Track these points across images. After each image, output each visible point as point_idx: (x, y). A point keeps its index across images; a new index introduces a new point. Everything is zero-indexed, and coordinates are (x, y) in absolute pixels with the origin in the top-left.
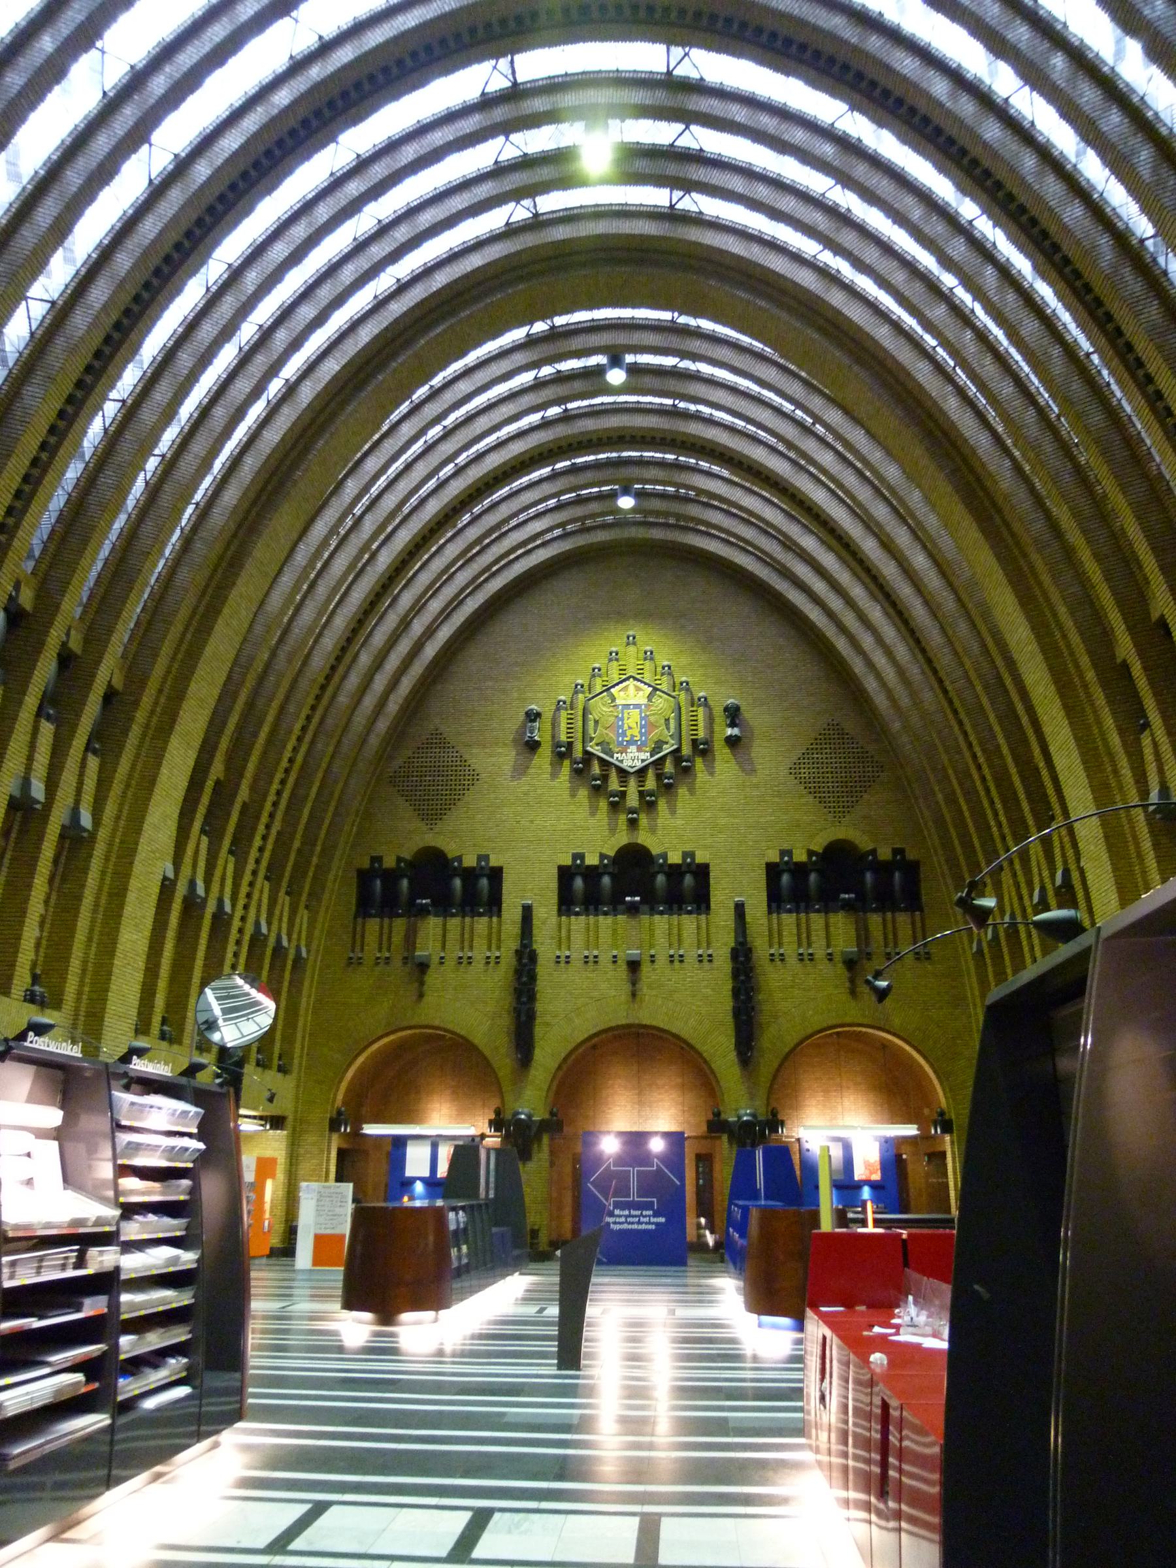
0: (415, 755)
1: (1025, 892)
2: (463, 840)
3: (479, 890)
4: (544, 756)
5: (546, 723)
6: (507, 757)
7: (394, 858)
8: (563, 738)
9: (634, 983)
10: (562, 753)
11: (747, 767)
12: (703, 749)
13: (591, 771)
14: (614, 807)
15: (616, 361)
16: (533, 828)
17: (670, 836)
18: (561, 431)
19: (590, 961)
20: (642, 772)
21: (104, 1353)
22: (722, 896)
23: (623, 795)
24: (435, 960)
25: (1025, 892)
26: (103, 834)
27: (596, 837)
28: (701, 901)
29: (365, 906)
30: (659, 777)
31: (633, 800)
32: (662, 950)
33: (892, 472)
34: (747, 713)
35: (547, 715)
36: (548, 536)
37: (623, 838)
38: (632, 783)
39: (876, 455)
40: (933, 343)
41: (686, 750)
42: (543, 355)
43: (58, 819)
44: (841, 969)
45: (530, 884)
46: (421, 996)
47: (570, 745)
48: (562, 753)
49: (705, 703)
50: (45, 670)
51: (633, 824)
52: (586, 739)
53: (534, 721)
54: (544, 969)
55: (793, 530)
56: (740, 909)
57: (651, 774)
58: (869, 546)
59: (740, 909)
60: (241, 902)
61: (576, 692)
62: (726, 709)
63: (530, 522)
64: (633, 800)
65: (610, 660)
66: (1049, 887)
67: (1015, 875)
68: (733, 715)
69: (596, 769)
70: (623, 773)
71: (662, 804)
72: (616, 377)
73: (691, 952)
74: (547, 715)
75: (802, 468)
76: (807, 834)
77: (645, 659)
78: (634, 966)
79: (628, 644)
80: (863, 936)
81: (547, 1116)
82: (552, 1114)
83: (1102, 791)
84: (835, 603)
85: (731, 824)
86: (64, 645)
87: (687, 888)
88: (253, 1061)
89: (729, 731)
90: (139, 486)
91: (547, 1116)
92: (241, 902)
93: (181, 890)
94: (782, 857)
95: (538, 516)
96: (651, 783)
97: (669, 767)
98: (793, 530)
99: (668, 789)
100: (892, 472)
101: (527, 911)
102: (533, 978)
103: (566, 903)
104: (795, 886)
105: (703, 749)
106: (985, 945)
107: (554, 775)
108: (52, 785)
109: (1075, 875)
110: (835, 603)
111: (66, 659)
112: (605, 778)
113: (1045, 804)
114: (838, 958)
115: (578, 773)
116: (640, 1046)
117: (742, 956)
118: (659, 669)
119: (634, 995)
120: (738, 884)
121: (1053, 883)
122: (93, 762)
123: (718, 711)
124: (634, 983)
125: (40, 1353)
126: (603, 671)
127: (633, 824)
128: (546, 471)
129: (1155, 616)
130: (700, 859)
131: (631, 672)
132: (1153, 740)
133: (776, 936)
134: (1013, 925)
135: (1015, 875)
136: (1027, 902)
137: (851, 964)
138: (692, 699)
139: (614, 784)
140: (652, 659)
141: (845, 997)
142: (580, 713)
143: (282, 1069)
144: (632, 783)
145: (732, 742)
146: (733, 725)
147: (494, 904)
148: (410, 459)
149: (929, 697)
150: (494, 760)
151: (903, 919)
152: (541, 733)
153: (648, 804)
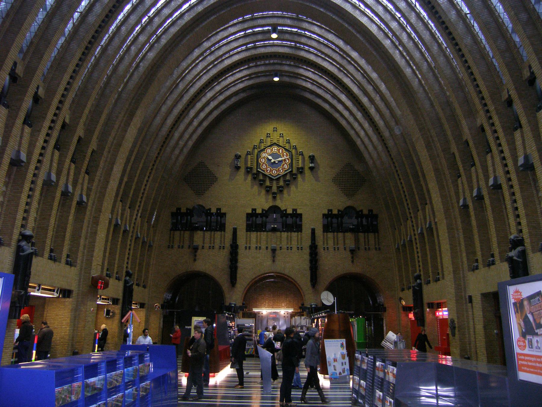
0: (198, 176)
1: (415, 228)
2: (213, 200)
3: (216, 221)
4: (243, 170)
5: (242, 160)
6: (228, 170)
7: (185, 208)
8: (249, 165)
9: (274, 257)
10: (249, 170)
11: (317, 179)
12: (301, 171)
13: (258, 177)
14: (267, 191)
15: (274, 31)
16: (237, 197)
17: (287, 202)
18: (254, 52)
19: (258, 248)
20: (278, 179)
21: (88, 378)
22: (307, 225)
23: (271, 187)
24: (200, 247)
25: (415, 228)
26: (90, 204)
27: (262, 203)
28: (298, 228)
29: (175, 228)
30: (285, 181)
31: (274, 189)
32: (284, 245)
33: (374, 75)
34: (318, 159)
35: (243, 157)
36: (239, 49)
37: (270, 203)
38: (275, 182)
39: (368, 69)
40: (399, 16)
41: (295, 171)
42: (251, 40)
43: (76, 199)
44: (349, 253)
45: (236, 219)
46: (195, 260)
47: (251, 168)
48: (249, 170)
49: (302, 154)
50: (28, 102)
51: (274, 198)
52: (258, 164)
53: (239, 158)
54: (320, 250)
55: (337, 92)
56: (313, 231)
57: (282, 180)
58: (365, 100)
59: (313, 231)
60: (132, 225)
61: (254, 148)
62: (310, 157)
63: (238, 80)
64: (274, 189)
65: (267, 137)
66: (424, 227)
67: (412, 222)
68: (312, 159)
69: (261, 177)
70: (271, 179)
71: (285, 192)
72: (274, 36)
73: (294, 244)
74: (243, 157)
75: (342, 71)
76: (339, 203)
77: (280, 137)
78: (274, 251)
79: (274, 131)
80: (357, 240)
81: (241, 305)
82: (243, 304)
83: (443, 197)
84: (351, 119)
85: (312, 199)
86: (36, 93)
87: (292, 222)
88: (135, 284)
89: (311, 165)
90: (70, 26)
91: (241, 305)
92: (132, 225)
93: (114, 222)
94: (252, 211)
95: (238, 53)
96: (281, 183)
97: (288, 177)
98: (337, 92)
99: (288, 184)
100: (374, 75)
101: (235, 231)
102: (316, 254)
103: (250, 228)
104: (333, 222)
105: (301, 171)
106: (406, 242)
107: (245, 179)
108: (59, 174)
109: (433, 223)
110: (351, 119)
111: (36, 99)
112: (264, 181)
113: (425, 200)
114: (348, 249)
115: (254, 178)
116: (277, 285)
117: (313, 248)
118: (285, 141)
119: (274, 261)
120: (312, 220)
121: (426, 226)
122: (73, 166)
123: (307, 158)
124: (274, 257)
125: (419, 385)
126: (264, 141)
127: (274, 198)
128: (240, 19)
129: (464, 139)
130: (299, 212)
131: (275, 141)
132: (462, 181)
133: (248, 240)
134: (411, 241)
135: (412, 222)
136: (416, 232)
137: (352, 251)
138: (297, 152)
139: (268, 183)
140: (283, 137)
141: (350, 263)
142: (256, 157)
143: (144, 287)
144: (275, 182)
145: (311, 169)
146: (311, 163)
147: (222, 227)
148: (198, 66)
149: (384, 156)
150: (224, 172)
151: (371, 236)
152: (241, 163)
153: (281, 190)
